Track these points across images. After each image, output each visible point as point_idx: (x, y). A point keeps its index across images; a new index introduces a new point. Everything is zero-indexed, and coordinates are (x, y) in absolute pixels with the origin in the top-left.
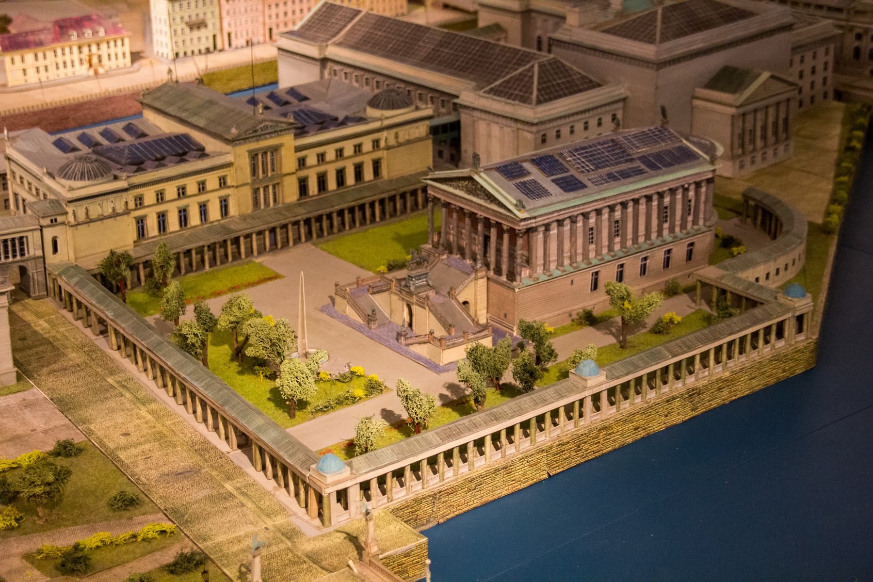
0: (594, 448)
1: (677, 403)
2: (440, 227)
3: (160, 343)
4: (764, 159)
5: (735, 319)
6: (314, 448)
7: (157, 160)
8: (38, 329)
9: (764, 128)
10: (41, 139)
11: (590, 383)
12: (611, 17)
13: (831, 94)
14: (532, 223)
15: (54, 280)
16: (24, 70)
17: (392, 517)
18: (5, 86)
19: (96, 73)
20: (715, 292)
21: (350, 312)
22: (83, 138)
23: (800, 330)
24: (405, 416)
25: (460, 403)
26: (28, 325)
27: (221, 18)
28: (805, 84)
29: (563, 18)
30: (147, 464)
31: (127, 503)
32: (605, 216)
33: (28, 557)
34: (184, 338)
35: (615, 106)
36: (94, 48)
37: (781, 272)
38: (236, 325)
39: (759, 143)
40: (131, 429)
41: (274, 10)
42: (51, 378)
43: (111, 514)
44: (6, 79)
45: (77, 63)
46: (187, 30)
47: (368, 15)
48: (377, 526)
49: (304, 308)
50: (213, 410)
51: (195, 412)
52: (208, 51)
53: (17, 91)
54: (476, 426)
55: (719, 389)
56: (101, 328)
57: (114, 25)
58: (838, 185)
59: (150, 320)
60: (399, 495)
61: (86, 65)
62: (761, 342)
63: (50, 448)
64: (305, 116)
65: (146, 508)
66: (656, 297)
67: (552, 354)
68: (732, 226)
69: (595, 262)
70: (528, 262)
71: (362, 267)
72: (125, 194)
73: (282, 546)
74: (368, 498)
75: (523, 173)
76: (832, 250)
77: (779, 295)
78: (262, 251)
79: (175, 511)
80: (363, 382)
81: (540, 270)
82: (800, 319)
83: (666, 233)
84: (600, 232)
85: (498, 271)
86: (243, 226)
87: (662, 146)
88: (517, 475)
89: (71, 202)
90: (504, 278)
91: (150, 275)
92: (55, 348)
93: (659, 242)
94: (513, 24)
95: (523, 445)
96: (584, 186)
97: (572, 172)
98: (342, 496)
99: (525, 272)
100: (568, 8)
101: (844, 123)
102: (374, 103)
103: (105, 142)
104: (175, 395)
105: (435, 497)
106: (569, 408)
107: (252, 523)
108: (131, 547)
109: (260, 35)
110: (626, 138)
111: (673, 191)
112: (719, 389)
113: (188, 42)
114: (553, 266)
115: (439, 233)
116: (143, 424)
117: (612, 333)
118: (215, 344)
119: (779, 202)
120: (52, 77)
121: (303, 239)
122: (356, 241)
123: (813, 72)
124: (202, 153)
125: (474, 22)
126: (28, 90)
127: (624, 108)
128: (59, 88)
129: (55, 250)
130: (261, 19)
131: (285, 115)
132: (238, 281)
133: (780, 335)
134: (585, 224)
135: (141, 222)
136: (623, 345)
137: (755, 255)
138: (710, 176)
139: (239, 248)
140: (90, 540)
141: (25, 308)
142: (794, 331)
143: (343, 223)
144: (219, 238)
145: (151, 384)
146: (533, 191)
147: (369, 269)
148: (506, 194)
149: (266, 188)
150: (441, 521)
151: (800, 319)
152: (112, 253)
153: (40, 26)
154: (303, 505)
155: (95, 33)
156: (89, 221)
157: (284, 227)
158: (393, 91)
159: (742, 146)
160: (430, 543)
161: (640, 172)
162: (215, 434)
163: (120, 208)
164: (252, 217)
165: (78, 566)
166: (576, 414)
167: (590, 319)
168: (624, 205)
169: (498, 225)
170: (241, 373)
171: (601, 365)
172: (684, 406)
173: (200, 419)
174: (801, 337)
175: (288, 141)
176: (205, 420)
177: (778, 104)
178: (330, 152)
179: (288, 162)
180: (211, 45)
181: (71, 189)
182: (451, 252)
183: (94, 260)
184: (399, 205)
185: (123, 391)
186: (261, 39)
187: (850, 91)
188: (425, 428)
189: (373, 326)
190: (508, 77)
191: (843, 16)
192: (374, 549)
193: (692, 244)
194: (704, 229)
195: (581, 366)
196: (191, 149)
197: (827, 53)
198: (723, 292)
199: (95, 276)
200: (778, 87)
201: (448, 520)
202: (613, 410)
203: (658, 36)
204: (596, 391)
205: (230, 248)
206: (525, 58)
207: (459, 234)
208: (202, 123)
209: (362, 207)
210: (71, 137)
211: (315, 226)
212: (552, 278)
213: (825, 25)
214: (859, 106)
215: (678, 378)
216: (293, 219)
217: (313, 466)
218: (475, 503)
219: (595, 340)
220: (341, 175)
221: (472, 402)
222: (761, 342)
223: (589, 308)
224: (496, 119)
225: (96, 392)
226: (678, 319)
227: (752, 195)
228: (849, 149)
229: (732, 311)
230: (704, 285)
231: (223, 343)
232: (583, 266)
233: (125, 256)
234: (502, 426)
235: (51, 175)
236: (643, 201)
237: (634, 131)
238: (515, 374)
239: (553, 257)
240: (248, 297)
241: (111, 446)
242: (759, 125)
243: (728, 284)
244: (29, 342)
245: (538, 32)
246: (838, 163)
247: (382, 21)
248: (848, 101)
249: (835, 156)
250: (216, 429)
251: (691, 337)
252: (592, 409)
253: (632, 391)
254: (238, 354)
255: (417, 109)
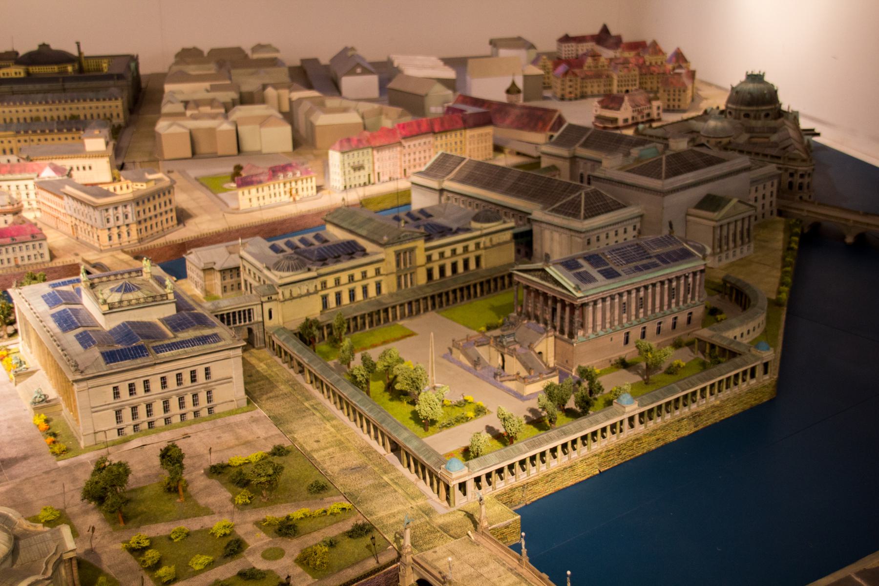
0: (630, 453)
1: (685, 422)
2: (522, 301)
3: (339, 380)
4: (734, 255)
5: (723, 365)
6: (442, 453)
7: (335, 257)
8: (259, 369)
9: (735, 235)
10: (261, 244)
11: (627, 409)
12: (631, 162)
13: (775, 212)
14: (585, 300)
15: (270, 337)
16: (250, 200)
17: (495, 500)
18: (238, 209)
19: (294, 199)
20: (708, 346)
21: (462, 359)
22: (289, 244)
23: (766, 372)
24: (502, 431)
25: (538, 422)
26: (253, 367)
27: (373, 163)
28: (759, 205)
29: (600, 162)
30: (332, 462)
31: (320, 489)
32: (634, 295)
33: (257, 523)
34: (355, 377)
35: (635, 220)
36: (293, 184)
37: (751, 333)
38: (388, 369)
39: (731, 245)
40: (321, 438)
41: (407, 157)
42: (269, 402)
43: (309, 495)
44: (239, 205)
45: (282, 193)
46: (352, 171)
47: (470, 161)
48: (486, 507)
49: (427, 352)
50: (374, 426)
51: (362, 426)
52: (365, 184)
53: (246, 213)
54: (552, 439)
55: (713, 412)
56: (299, 369)
57: (306, 169)
58: (785, 273)
59: (331, 363)
60: (500, 486)
61: (288, 195)
62: (740, 380)
63: (269, 450)
64: (431, 228)
65: (333, 492)
66: (669, 350)
67: (600, 388)
68: (716, 301)
69: (626, 325)
70: (583, 326)
71: (469, 328)
72: (315, 281)
73: (423, 520)
74: (480, 488)
75: (578, 266)
76: (783, 317)
77: (752, 349)
78: (403, 317)
79: (351, 495)
80: (473, 407)
81: (590, 331)
82: (766, 365)
83: (673, 306)
84: (630, 306)
85: (562, 332)
86: (390, 300)
87: (670, 248)
88: (579, 471)
89: (281, 286)
90: (566, 337)
91: (330, 334)
92: (270, 382)
93: (669, 312)
94: (564, 166)
95: (582, 451)
96: (619, 275)
97: (611, 265)
98: (462, 486)
99: (580, 333)
100: (603, 156)
101: (785, 231)
102: (476, 219)
103: (302, 246)
104: (348, 415)
105: (524, 487)
106: (613, 426)
107: (402, 504)
108: (323, 519)
109: (398, 173)
110: (646, 243)
111: (678, 278)
112: (713, 412)
113: (352, 179)
114: (599, 328)
115: (522, 306)
116: (329, 435)
117: (638, 374)
118: (375, 380)
119: (747, 285)
120: (267, 203)
121: (430, 308)
122: (464, 310)
123: (764, 197)
124: (364, 252)
125: (539, 164)
126: (252, 211)
127: (641, 222)
128: (272, 210)
129: (270, 317)
130: (399, 164)
131: (418, 227)
132: (387, 337)
133: (753, 376)
134: (620, 300)
135: (325, 298)
136: (647, 382)
137: (734, 321)
138: (703, 268)
139: (388, 315)
140: (297, 513)
141: (251, 356)
142: (762, 372)
143: (456, 298)
144: (375, 309)
145: (333, 407)
146: (585, 278)
147: (474, 329)
148: (568, 281)
149: (406, 275)
150: (528, 503)
151: (766, 365)
152: (307, 320)
153: (260, 171)
154: (436, 491)
155: (294, 174)
156: (292, 298)
157: (418, 301)
158: (487, 211)
159: (720, 247)
160: (522, 519)
161: (655, 265)
162: (375, 442)
163: (312, 290)
164: (397, 295)
165: (290, 531)
166: (618, 430)
167: (623, 364)
168: (646, 287)
169: (563, 301)
170: (391, 400)
171: (634, 397)
172: (689, 424)
173: (366, 431)
174: (767, 377)
175: (421, 244)
176: (369, 432)
177: (743, 219)
178: (448, 251)
179: (420, 258)
180: (366, 180)
181: (281, 278)
182: (530, 319)
183: (295, 324)
184: (492, 286)
185: (315, 412)
186: (399, 176)
187: (789, 210)
188: (516, 439)
189: (478, 368)
190: (564, 201)
191: (781, 161)
192: (485, 524)
193: (691, 313)
194: (698, 303)
195: (621, 398)
196: (357, 250)
197: (772, 185)
198: (713, 346)
199: (295, 334)
200: (743, 207)
201: (533, 502)
202: (642, 427)
203: (663, 175)
204: (631, 414)
205: (382, 315)
206: (578, 188)
207: (535, 306)
208: (364, 233)
209: (468, 287)
210: (281, 243)
211: (437, 300)
212: (598, 336)
213: (771, 168)
214: (794, 220)
215: (685, 405)
216: (423, 296)
217: (443, 466)
218: (550, 491)
219: (627, 380)
220: (454, 266)
221: (547, 421)
222: (740, 380)
223: (623, 357)
224: (556, 229)
225: (297, 412)
226: (683, 364)
227: (728, 280)
228: (789, 249)
229: (721, 359)
230: (699, 340)
231: (379, 379)
232: (619, 328)
233: (315, 322)
234: (568, 439)
235: (268, 268)
236: (658, 285)
237: (652, 237)
238: (576, 403)
239: (599, 322)
240: (396, 349)
241: (308, 449)
242: (731, 232)
243: (717, 341)
244: (254, 378)
245: (581, 171)
246: (783, 258)
247: (479, 165)
248: (786, 217)
249: (781, 253)
250: (376, 438)
251: (694, 377)
252: (626, 429)
253: (655, 415)
254: (390, 387)
255: (505, 222)
